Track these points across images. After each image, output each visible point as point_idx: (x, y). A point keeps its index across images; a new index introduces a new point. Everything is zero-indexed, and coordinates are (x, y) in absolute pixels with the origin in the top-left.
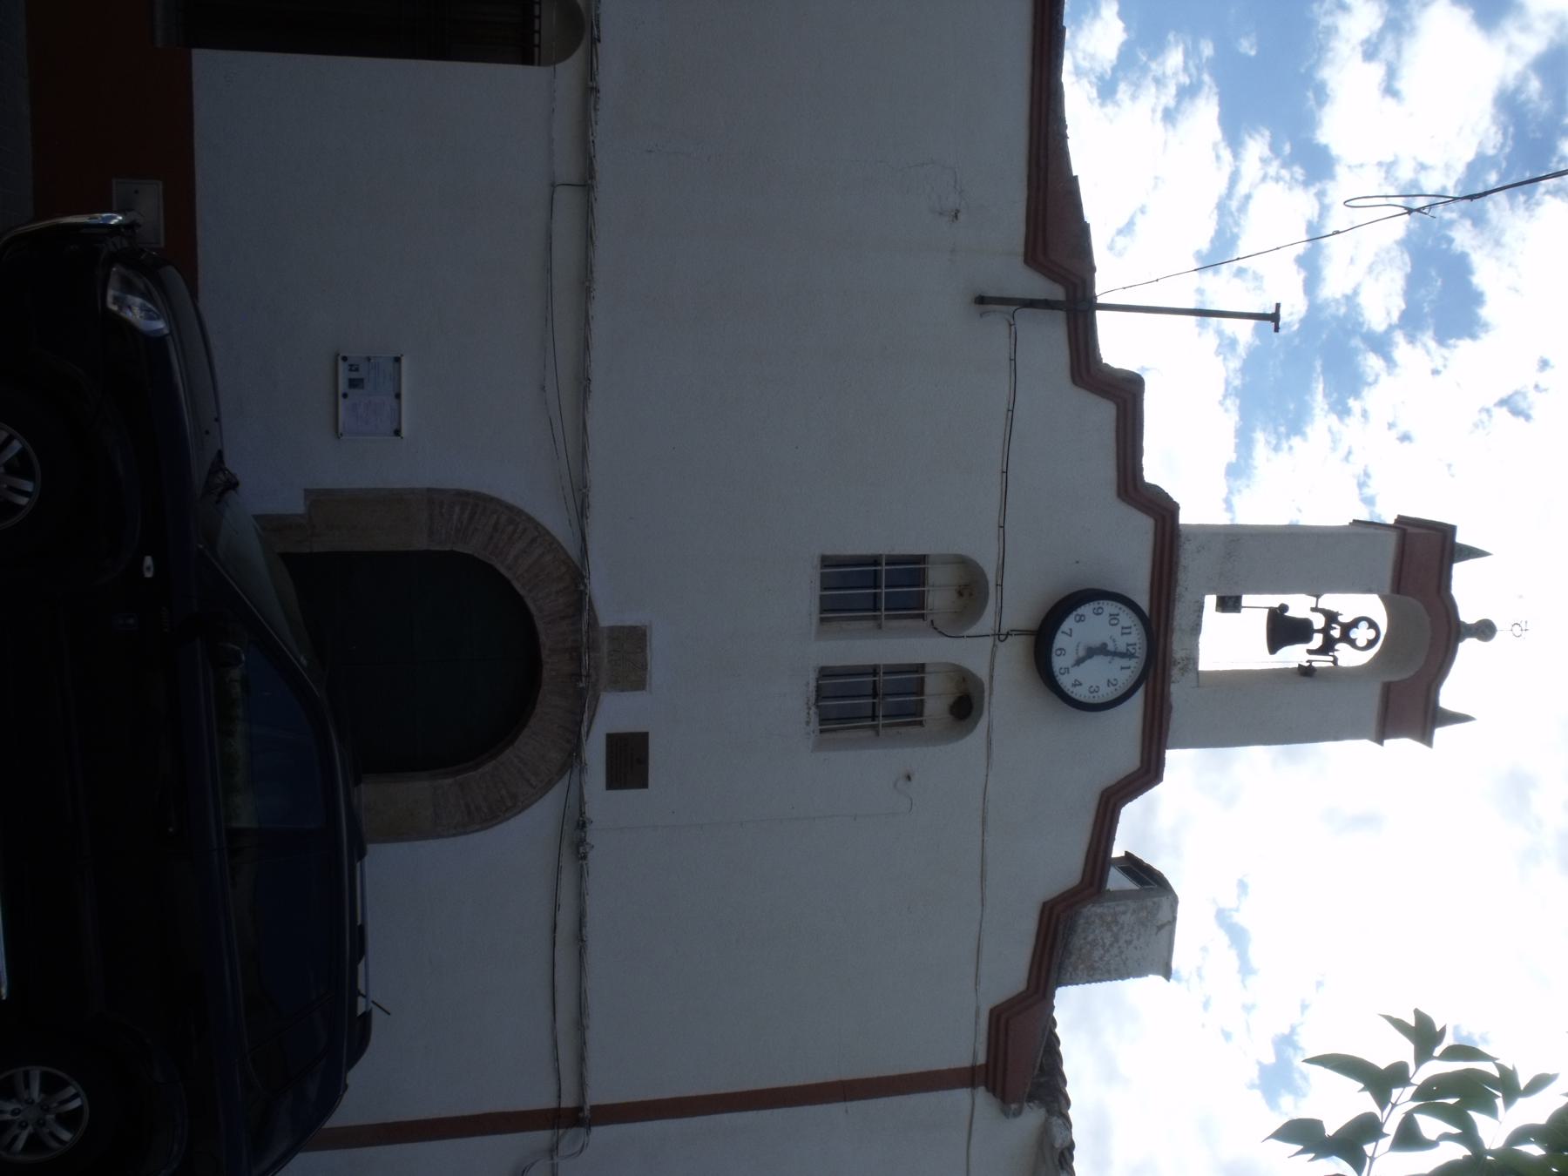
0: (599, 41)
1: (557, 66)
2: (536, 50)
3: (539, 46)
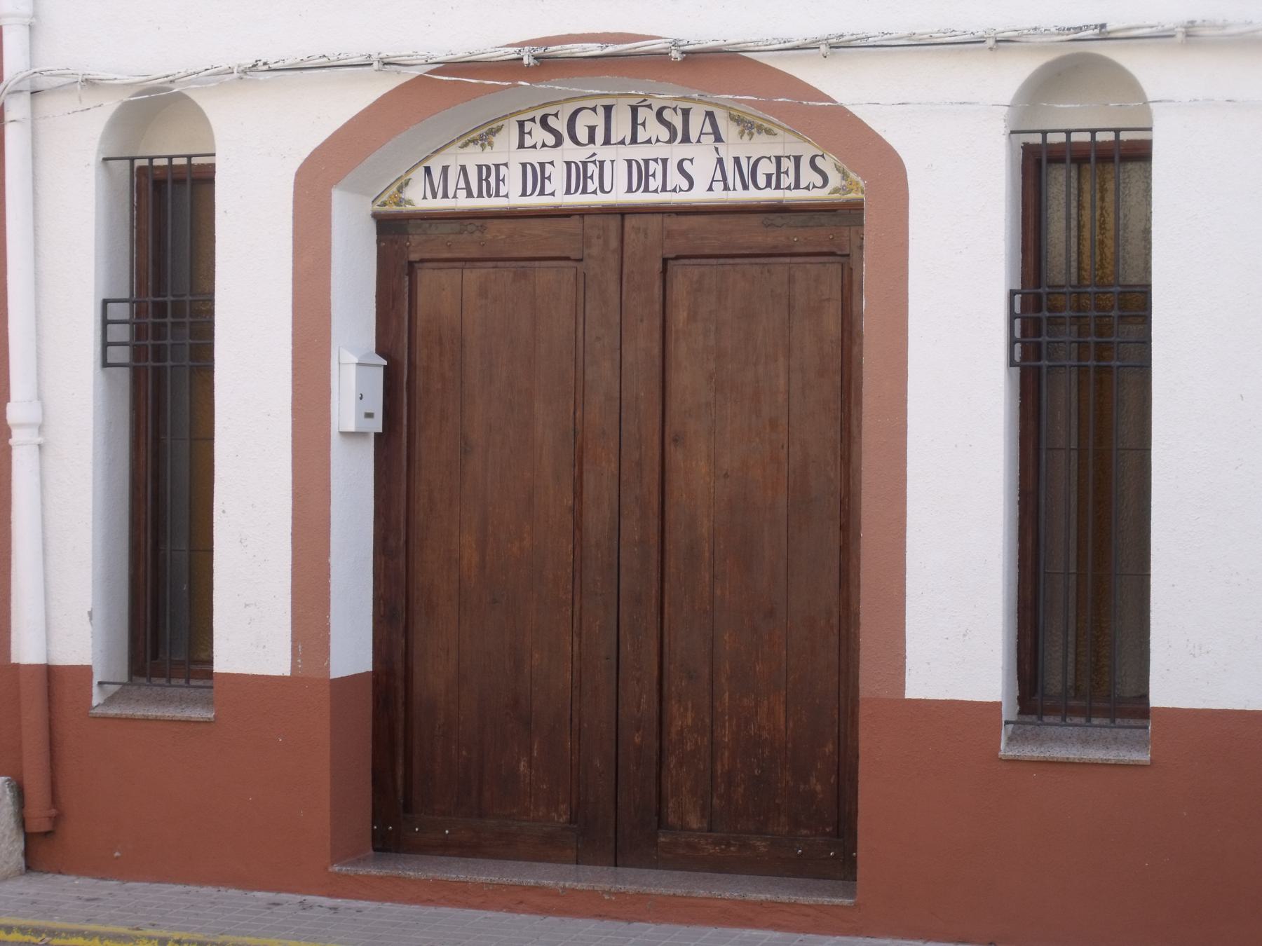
0: (1103, 26)
1: (1150, 99)
2: (1124, 136)
3: (1117, 131)
